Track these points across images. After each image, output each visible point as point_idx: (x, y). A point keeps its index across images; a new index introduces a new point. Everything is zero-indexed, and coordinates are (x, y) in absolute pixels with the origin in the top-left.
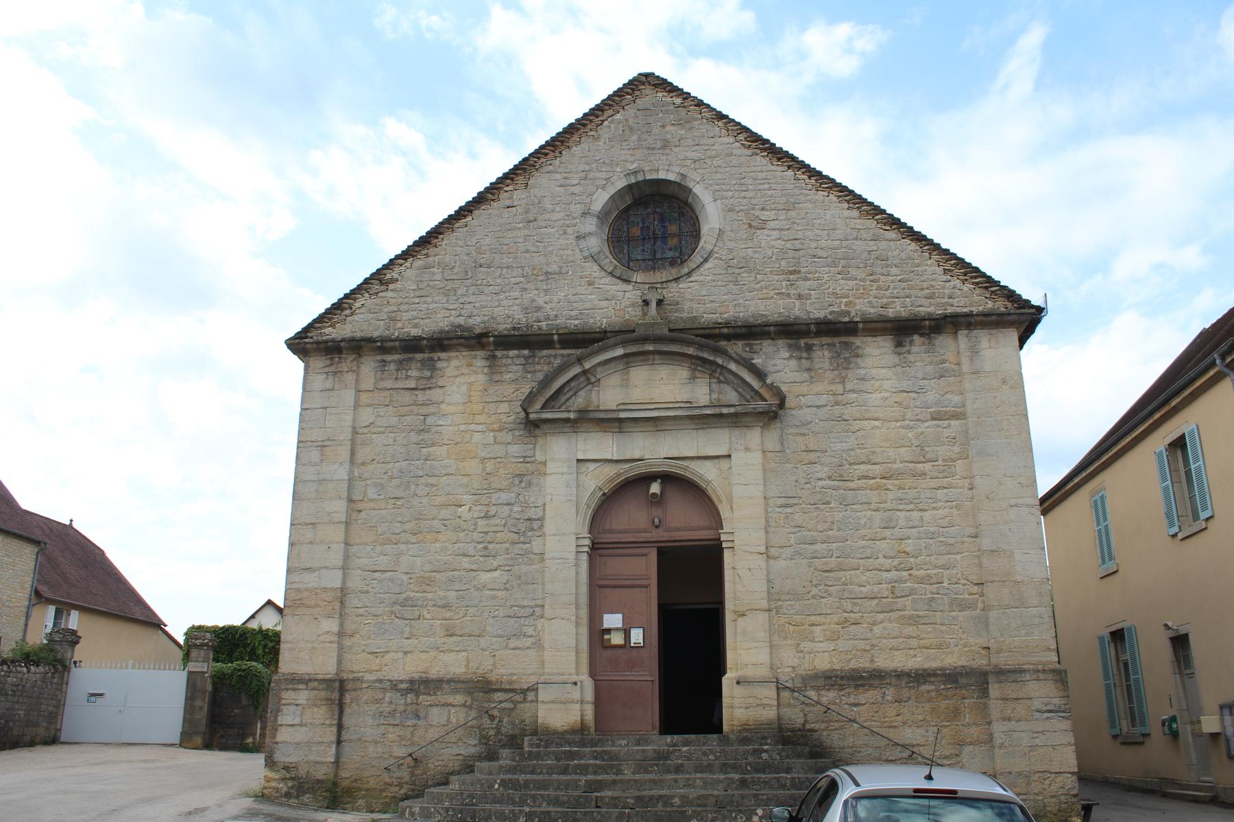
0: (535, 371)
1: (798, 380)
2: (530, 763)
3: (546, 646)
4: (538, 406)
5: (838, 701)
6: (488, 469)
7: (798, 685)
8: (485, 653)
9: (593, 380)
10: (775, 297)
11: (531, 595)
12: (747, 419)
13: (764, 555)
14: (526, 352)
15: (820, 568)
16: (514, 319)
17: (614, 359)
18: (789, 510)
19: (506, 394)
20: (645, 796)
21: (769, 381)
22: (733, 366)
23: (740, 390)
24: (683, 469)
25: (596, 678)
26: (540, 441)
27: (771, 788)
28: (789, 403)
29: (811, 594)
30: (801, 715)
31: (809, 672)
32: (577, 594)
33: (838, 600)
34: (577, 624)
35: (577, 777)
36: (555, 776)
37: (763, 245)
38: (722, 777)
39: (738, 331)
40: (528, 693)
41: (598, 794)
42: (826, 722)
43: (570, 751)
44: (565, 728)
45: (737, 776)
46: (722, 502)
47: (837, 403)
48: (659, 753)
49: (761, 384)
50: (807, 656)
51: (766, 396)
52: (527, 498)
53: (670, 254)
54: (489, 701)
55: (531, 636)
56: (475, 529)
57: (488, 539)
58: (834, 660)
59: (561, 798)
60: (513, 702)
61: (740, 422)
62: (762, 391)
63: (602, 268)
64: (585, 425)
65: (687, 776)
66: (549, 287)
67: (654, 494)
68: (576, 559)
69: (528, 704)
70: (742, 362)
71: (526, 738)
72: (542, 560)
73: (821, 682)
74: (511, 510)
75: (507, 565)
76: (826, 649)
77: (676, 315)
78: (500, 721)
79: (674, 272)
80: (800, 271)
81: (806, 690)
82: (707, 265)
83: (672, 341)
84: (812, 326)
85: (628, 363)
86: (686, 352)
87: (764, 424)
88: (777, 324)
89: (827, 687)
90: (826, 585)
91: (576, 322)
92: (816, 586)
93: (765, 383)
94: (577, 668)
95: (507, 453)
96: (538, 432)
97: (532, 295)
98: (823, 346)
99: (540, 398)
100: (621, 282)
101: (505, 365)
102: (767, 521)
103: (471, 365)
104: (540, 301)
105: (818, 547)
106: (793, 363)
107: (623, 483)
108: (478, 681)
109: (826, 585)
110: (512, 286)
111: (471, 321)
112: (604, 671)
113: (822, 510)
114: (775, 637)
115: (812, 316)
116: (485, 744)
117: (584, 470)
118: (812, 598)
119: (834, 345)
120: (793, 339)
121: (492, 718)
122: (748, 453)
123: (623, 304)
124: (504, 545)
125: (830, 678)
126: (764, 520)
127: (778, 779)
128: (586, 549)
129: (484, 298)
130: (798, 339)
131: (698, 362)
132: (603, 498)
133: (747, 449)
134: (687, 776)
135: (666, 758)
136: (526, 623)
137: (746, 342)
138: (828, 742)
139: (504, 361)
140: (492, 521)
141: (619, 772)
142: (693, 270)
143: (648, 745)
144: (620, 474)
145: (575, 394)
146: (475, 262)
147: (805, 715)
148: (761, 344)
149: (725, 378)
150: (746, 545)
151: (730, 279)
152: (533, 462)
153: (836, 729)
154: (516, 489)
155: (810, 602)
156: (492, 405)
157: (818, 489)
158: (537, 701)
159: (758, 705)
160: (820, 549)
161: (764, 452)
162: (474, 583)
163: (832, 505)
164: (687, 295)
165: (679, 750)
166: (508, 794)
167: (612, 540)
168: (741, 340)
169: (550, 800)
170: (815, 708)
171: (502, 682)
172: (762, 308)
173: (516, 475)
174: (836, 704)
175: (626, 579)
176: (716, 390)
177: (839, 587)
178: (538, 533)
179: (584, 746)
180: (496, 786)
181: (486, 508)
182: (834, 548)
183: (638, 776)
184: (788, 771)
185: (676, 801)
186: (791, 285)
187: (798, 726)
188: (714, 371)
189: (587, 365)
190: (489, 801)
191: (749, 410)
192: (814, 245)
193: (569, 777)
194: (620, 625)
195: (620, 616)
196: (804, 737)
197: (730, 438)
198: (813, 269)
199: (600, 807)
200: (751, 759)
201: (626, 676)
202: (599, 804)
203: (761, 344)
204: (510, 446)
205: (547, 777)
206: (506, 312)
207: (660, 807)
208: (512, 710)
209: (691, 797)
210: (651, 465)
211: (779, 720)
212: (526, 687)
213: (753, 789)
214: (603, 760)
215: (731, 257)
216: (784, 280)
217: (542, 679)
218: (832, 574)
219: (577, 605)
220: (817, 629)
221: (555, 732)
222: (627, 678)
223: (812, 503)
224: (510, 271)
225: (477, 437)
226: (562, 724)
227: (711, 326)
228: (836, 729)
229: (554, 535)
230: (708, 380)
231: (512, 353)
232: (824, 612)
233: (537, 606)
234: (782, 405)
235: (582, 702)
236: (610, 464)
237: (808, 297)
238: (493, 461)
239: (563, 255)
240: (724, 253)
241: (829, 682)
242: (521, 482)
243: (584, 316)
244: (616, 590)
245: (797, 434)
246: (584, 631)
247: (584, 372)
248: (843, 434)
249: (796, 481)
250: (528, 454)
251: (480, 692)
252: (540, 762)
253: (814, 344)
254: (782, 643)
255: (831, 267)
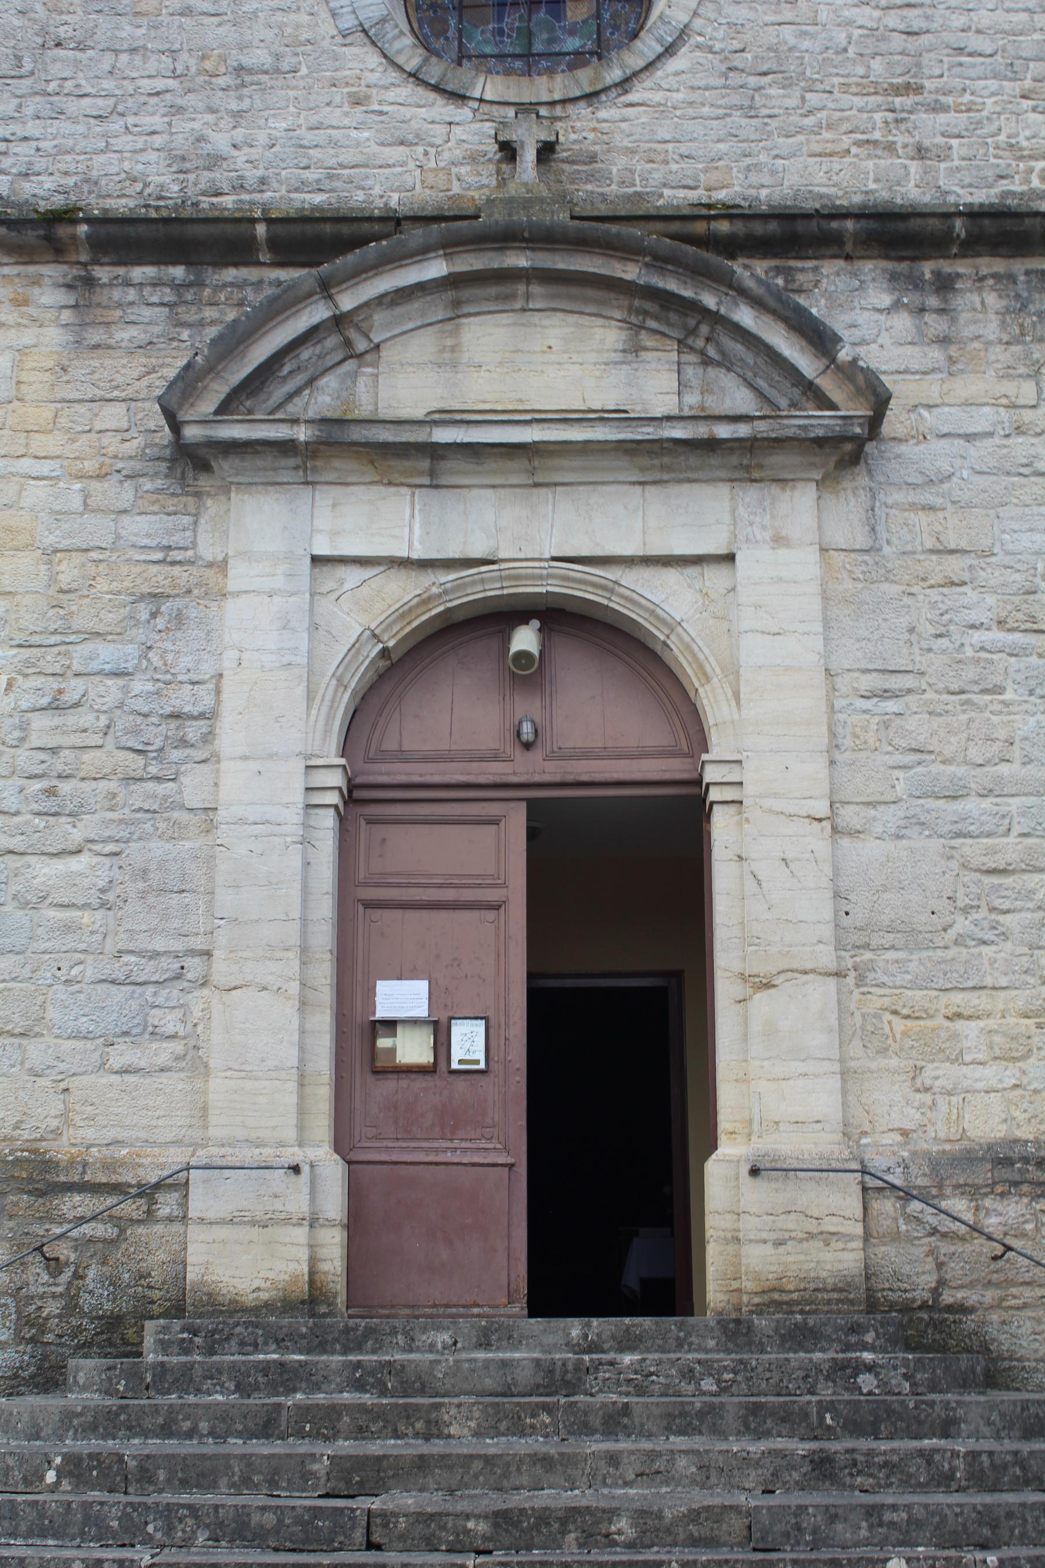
0: (201, 324)
1: (915, 366)
2: (159, 1400)
3: (212, 1064)
4: (207, 406)
5: (1029, 1227)
6: (65, 580)
7: (920, 1182)
8: (42, 1082)
9: (361, 345)
10: (854, 150)
11: (176, 924)
12: (777, 458)
13: (826, 824)
14: (178, 272)
15: (974, 863)
16: (146, 185)
17: (421, 288)
18: (891, 706)
19: (119, 379)
20: (522, 1511)
21: (844, 355)
22: (745, 316)
23: (761, 383)
24: (604, 588)
25: (354, 1156)
26: (212, 506)
27: (909, 1484)
28: (894, 422)
29: (952, 933)
30: (930, 1265)
31: (948, 1147)
32: (304, 921)
33: (1026, 950)
34: (303, 1004)
35: (304, 1447)
36: (236, 1445)
37: (823, 17)
38: (756, 1447)
39: (758, 228)
40: (160, 1197)
41: (375, 1504)
42: (997, 1285)
43: (282, 1364)
44: (264, 1296)
45: (802, 1448)
46: (708, 680)
47: (1019, 430)
48: (551, 1372)
49: (821, 364)
50: (941, 1101)
51: (836, 395)
52: (170, 657)
53: (572, 43)
54: (48, 1218)
55: (174, 1037)
56: (22, 739)
57: (60, 767)
58: (1017, 1113)
59: (255, 1518)
60: (115, 1220)
61: (761, 467)
62: (827, 384)
63: (392, 63)
64: (336, 463)
65: (646, 1445)
66: (246, 104)
67: (523, 655)
68: (306, 826)
69: (159, 1228)
70: (772, 303)
71: (149, 1325)
72: (210, 828)
73: (983, 1174)
74: (125, 689)
75: (111, 839)
76: (994, 1083)
77: (589, 187)
78: (77, 1276)
79: (584, 79)
80: (922, 87)
81: (942, 1196)
82: (674, 64)
83: (581, 243)
84: (958, 224)
85: (457, 304)
86: (619, 274)
87: (823, 479)
88: (860, 214)
89: (999, 1189)
90: (993, 909)
91: (318, 199)
92: (966, 910)
93: (833, 360)
94: (301, 1128)
95: (118, 537)
96: (204, 482)
97: (196, 125)
98: (982, 279)
99: (215, 386)
100: (440, 100)
101: (119, 305)
102: (832, 734)
103: (26, 302)
104: (220, 141)
105: (972, 806)
106: (902, 322)
107: (438, 626)
108: (18, 1161)
109: (993, 909)
110: (143, 99)
111: (28, 189)
112: (377, 1138)
113: (981, 709)
114: (855, 1048)
115: (951, 199)
116: (32, 1340)
117: (330, 585)
118: (956, 942)
119: (1012, 278)
120: (902, 259)
121: (54, 1266)
122: (783, 552)
123: (446, 155)
124: (103, 784)
125: (1007, 1162)
126: (824, 729)
127: (928, 1456)
128: (333, 798)
129: (64, 126)
130: (913, 259)
131: (648, 306)
132: (383, 664)
133: (779, 540)
134: (646, 1445)
135: (572, 1387)
136: (160, 1000)
137: (774, 263)
138: (1004, 1342)
139: (116, 294)
140: (72, 719)
141: (433, 1430)
142: (635, 74)
143: (515, 1348)
144: (429, 600)
145: (310, 382)
146: (44, 32)
147: (940, 1266)
148: (816, 269)
149: (722, 352)
150: (775, 795)
151: (736, 99)
152: (191, 562)
153: (1025, 1306)
154: (140, 634)
155: (950, 954)
156: (81, 408)
157: (969, 652)
158: (184, 1218)
159: (811, 1236)
160: (975, 813)
161: (823, 550)
162: (13, 888)
163: (1008, 696)
164: (618, 137)
165: (612, 1363)
166: (87, 1506)
167: (402, 779)
168: (765, 256)
169: (221, 1525)
170: (968, 1247)
171: (85, 1165)
172: (820, 177)
173: (142, 597)
174: (1024, 1235)
175: (440, 886)
176: (695, 382)
177: (1029, 915)
178: (200, 755)
179: (323, 1347)
180: (51, 1477)
181: (54, 684)
182: (1014, 809)
183: (492, 1446)
184: (947, 1428)
185: (623, 1526)
186: (897, 121)
187: (921, 1295)
188: (693, 332)
189: (347, 302)
190: (23, 1528)
191: (790, 432)
192: (959, 21)
193: (278, 1448)
194: (421, 1011)
195: (420, 988)
196: (938, 1325)
197: (733, 510)
198: (958, 83)
199: (378, 1547)
200: (826, 1392)
201: (437, 1150)
202: (376, 1538)
203: (816, 269)
204: (126, 520)
205: (210, 1447)
206: (127, 166)
207: (570, 1550)
208: (112, 1243)
209: (668, 1514)
210: (517, 577)
211: (868, 1278)
212: (153, 1180)
213: (852, 1487)
214: (384, 1392)
215: (736, 45)
216: (878, 108)
217: (202, 1156)
218: (1008, 881)
219: (304, 950)
220: (970, 1030)
221: (235, 1308)
222: (440, 1158)
223: (954, 687)
224: (137, 59)
225: (36, 493)
226: (256, 1284)
227: (686, 211)
228: (1025, 1306)
229: (245, 758)
230: (674, 356)
231: (140, 273)
232: (988, 981)
233: (192, 953)
234: (875, 422)
235: (314, 1222)
236: (403, 573)
237: (943, 154)
238: (78, 558)
239: (285, 25)
240: (720, 34)
241: (1006, 1173)
242: (154, 615)
243: (338, 184)
244: (412, 915)
245: (913, 507)
246: (323, 1022)
247: (339, 321)
248: (1036, 509)
249: (912, 630)
250: (177, 539)
251: (23, 1191)
252: (191, 1399)
253: (958, 276)
254: (873, 1065)
255: (1005, 78)
